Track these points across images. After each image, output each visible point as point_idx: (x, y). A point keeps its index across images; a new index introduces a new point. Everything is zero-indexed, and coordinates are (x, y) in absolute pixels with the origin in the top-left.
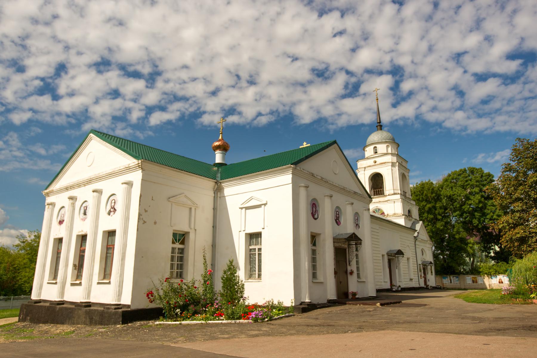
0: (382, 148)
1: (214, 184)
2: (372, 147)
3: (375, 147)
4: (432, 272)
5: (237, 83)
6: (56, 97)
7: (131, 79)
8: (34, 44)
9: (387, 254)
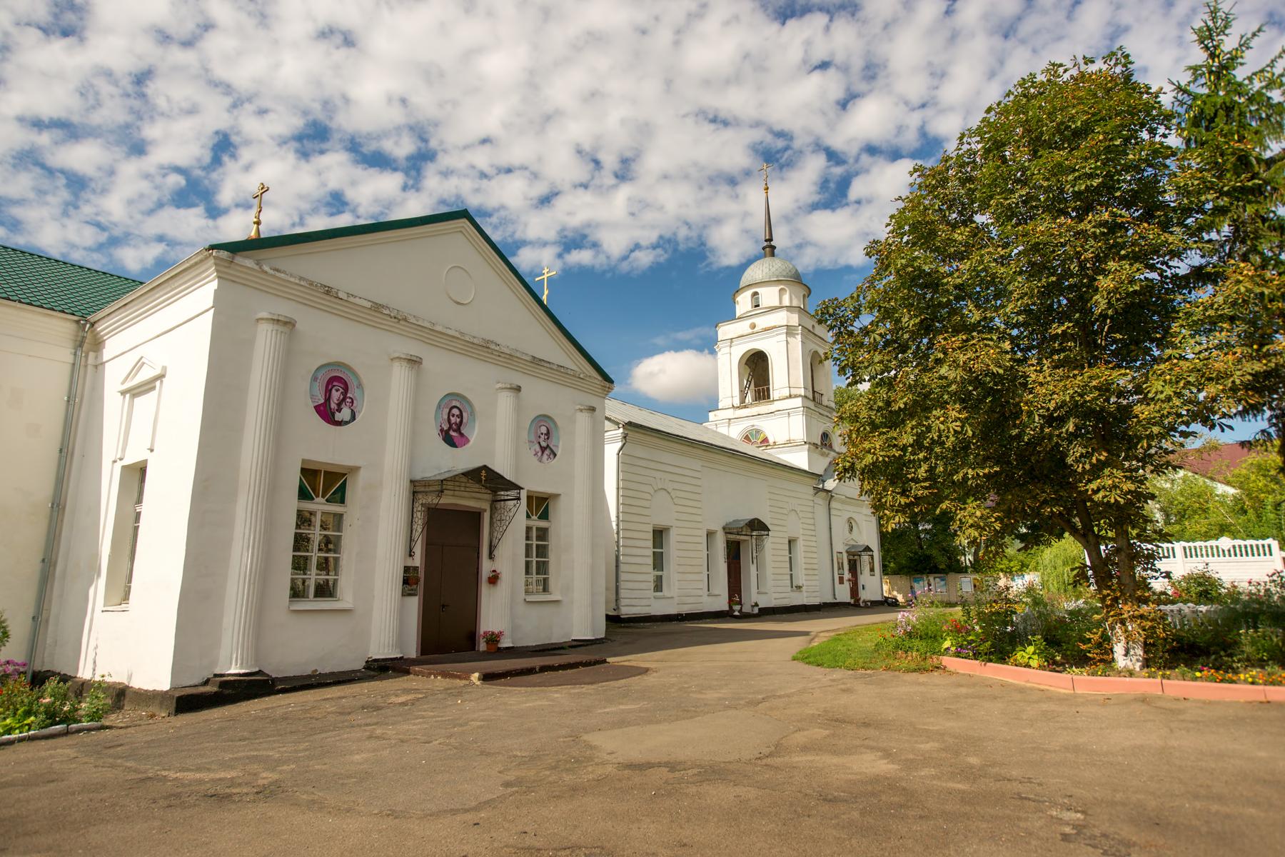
0: (769, 296)
1: (73, 326)
2: (748, 293)
3: (756, 294)
4: (872, 570)
5: (593, 178)
6: (215, 212)
7: (372, 171)
8: (164, 91)
9: (724, 528)
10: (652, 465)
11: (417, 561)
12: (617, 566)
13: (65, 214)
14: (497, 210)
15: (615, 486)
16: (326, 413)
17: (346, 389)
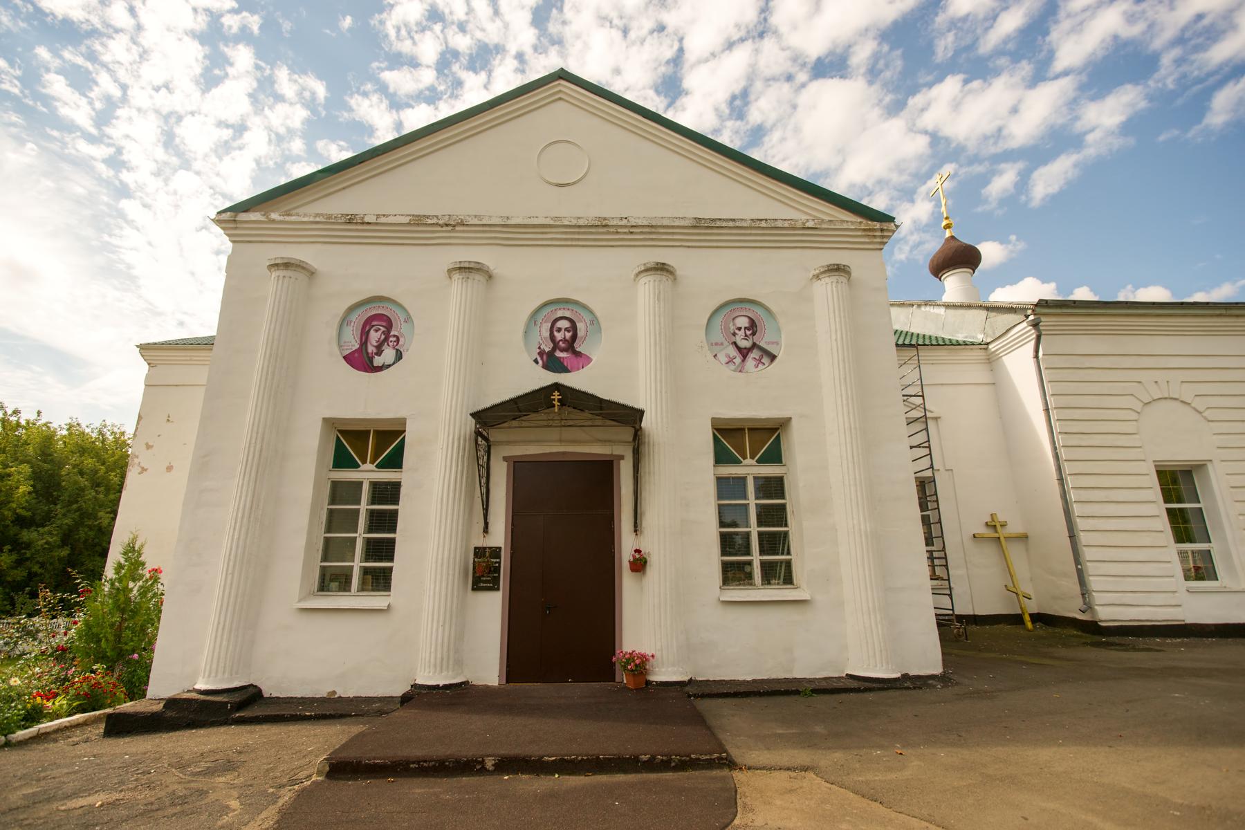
11: (498, 537)
12: (1072, 536)
15: (1041, 407)
16: (362, 361)
17: (389, 324)
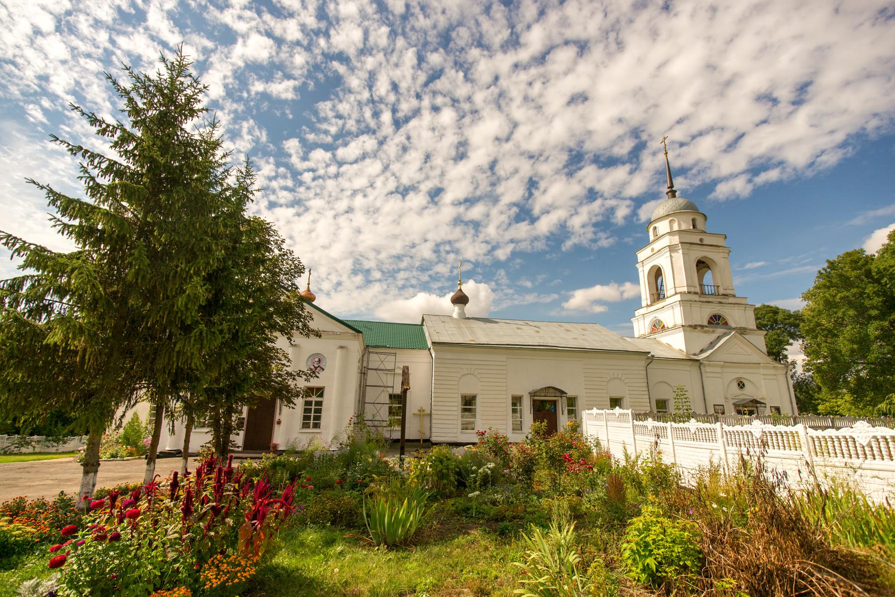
6: (533, 220)
10: (460, 362)
13: (474, 241)
14: (696, 164)
